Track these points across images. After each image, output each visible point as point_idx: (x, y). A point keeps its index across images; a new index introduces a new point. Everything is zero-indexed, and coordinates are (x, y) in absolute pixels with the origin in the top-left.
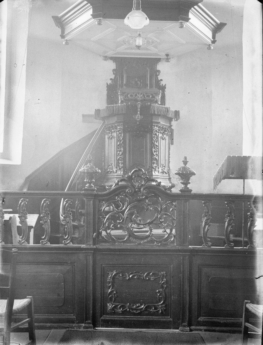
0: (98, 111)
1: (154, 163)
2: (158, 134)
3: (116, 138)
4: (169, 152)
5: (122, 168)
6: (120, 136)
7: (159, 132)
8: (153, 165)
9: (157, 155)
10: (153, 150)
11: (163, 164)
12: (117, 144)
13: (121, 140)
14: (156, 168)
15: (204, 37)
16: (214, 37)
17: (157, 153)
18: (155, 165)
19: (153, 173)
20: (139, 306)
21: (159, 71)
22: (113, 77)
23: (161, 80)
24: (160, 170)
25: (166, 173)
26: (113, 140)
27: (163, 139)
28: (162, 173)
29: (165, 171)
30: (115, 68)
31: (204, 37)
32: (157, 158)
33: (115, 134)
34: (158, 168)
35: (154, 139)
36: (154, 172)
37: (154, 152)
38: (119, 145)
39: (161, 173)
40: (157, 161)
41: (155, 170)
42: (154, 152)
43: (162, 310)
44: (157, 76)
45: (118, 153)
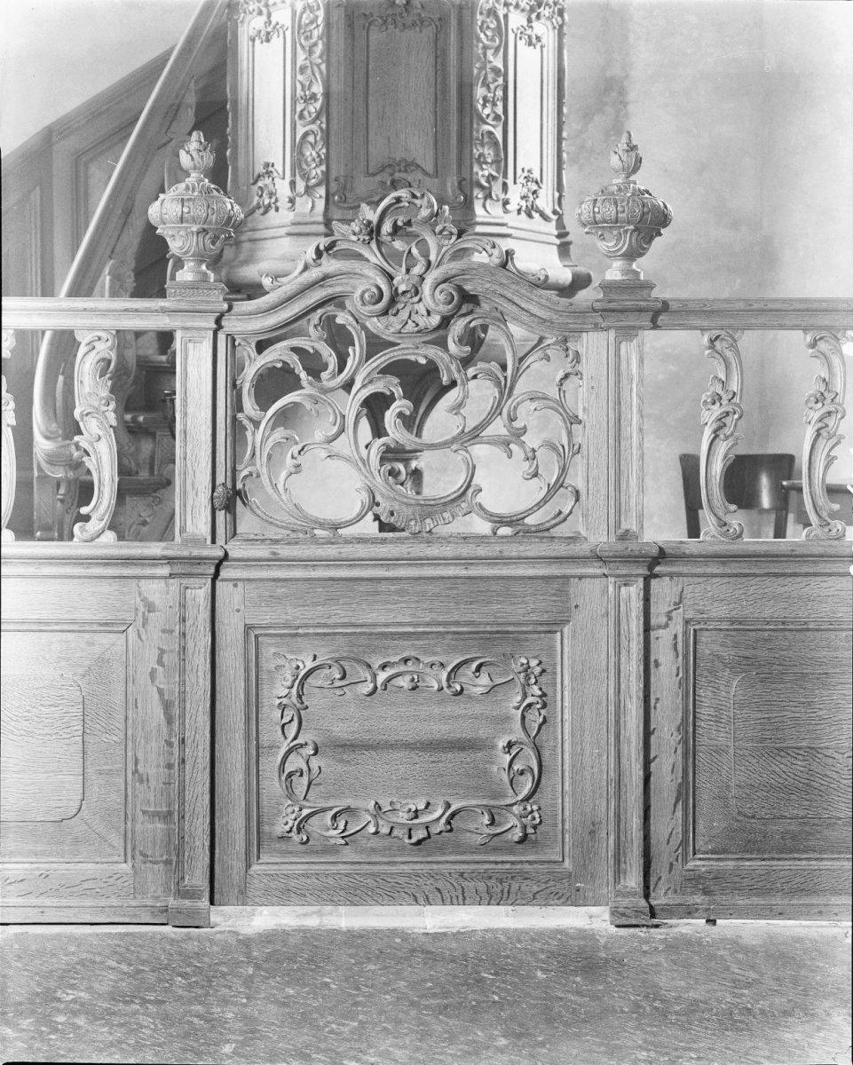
1: (481, 161)
2: (506, 16)
3: (289, 34)
5: (318, 184)
6: (311, 22)
8: (476, 169)
9: (497, 118)
10: (480, 92)
13: (315, 44)
14: (490, 188)
17: (499, 110)
18: (489, 170)
19: (479, 210)
20: (416, 814)
25: (543, 215)
26: (277, 41)
27: (530, 44)
28: (523, 213)
32: (498, 134)
35: (482, 36)
36: (484, 206)
37: (484, 106)
38: (303, 70)
39: (519, 211)
40: (497, 155)
41: (488, 196)
42: (484, 106)
43: (524, 827)
45: (299, 108)
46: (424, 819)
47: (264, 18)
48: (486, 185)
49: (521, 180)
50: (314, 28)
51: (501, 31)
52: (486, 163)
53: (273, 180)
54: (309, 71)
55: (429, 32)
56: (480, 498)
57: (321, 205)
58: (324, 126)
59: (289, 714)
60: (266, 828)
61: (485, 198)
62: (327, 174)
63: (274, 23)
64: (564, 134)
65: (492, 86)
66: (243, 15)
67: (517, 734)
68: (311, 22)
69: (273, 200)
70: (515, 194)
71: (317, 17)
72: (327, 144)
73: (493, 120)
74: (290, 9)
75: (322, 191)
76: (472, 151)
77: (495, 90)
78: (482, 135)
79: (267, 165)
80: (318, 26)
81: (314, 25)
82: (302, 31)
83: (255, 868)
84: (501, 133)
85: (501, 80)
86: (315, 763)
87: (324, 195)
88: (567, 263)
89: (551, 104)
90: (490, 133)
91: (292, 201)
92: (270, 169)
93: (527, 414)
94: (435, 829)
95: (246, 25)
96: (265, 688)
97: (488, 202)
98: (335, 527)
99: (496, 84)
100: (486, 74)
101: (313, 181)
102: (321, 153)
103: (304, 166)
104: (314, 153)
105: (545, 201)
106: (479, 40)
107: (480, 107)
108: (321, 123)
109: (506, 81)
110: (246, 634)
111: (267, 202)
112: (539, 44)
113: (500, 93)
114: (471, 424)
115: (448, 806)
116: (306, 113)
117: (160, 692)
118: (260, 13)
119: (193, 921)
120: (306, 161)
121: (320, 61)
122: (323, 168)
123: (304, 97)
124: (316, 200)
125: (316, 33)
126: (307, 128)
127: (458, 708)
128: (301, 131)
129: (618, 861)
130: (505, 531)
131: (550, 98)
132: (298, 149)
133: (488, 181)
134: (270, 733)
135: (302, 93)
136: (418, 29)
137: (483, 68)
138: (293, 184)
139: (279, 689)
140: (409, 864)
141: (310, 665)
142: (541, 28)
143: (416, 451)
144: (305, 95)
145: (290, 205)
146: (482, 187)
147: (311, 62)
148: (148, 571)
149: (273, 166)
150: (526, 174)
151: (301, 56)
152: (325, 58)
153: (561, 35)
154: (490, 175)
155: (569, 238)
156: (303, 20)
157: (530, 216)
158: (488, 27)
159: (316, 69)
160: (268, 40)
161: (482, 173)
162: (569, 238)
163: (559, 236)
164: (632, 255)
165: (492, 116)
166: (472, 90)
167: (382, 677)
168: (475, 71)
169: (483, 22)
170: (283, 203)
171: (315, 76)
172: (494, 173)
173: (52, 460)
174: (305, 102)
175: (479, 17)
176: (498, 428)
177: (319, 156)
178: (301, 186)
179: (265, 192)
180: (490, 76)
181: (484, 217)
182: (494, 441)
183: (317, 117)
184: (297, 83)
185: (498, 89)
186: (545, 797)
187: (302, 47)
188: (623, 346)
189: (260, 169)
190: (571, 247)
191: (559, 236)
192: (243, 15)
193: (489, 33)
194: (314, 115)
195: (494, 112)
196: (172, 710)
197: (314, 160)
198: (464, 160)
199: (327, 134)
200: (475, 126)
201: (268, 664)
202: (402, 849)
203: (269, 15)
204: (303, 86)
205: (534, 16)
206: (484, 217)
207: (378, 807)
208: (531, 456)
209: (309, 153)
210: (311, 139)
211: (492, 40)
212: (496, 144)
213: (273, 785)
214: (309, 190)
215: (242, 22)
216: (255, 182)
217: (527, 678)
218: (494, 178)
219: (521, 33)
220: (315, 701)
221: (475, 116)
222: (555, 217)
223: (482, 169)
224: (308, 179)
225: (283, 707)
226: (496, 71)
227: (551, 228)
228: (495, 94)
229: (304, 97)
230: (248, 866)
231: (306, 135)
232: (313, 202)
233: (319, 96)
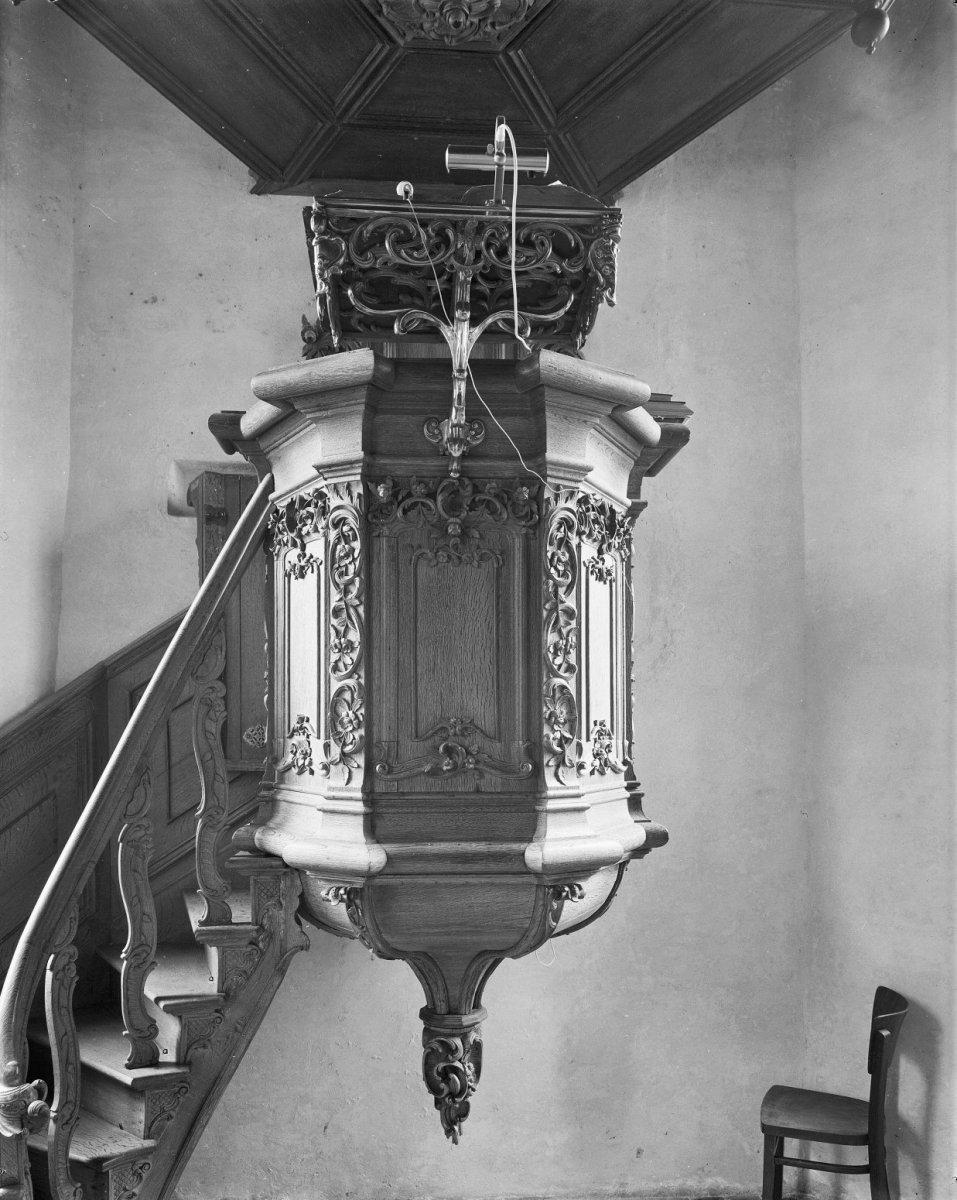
2: (579, 546)
3: (322, 567)
6: (347, 555)
7: (580, 534)
8: (546, 730)
10: (551, 638)
11: (602, 724)
13: (352, 582)
14: (563, 753)
16: (634, 490)
17: (572, 658)
24: (587, 757)
25: (615, 770)
26: (311, 578)
33: (316, 548)
34: (580, 750)
35: (553, 571)
37: (556, 654)
38: (337, 612)
39: (592, 773)
40: (570, 712)
41: (561, 762)
45: (334, 657)
47: (298, 551)
48: (559, 749)
49: (593, 736)
50: (350, 563)
51: (573, 564)
52: (557, 722)
53: (308, 737)
54: (344, 615)
58: (362, 681)
61: (558, 767)
63: (308, 556)
64: (633, 676)
65: (564, 631)
66: (278, 547)
68: (347, 555)
69: (307, 763)
70: (587, 757)
71: (354, 550)
72: (368, 703)
73: (565, 672)
74: (323, 539)
75: (360, 760)
76: (541, 709)
77: (568, 636)
78: (554, 690)
79: (301, 720)
80: (354, 560)
81: (350, 559)
82: (337, 565)
84: (574, 685)
85: (574, 623)
87: (363, 765)
88: (638, 818)
90: (563, 687)
91: (326, 767)
92: (305, 724)
95: (281, 557)
97: (561, 769)
99: (569, 628)
100: (557, 617)
101: (351, 747)
102: (359, 713)
103: (340, 729)
104: (350, 713)
105: (615, 758)
106: (550, 576)
107: (551, 657)
108: (359, 677)
109: (579, 624)
111: (301, 762)
112: (609, 578)
113: (573, 638)
116: (341, 665)
118: (295, 545)
120: (341, 723)
121: (357, 602)
122: (362, 732)
123: (339, 646)
124: (353, 769)
125: (351, 569)
126: (340, 684)
128: (335, 686)
131: (620, 638)
132: (333, 707)
133: (560, 745)
135: (337, 641)
136: (475, 563)
137: (555, 608)
138: (327, 747)
142: (610, 561)
143: (361, 127)
144: (340, 643)
145: (324, 772)
146: (554, 754)
147: (346, 604)
149: (308, 721)
150: (598, 728)
151: (335, 596)
152: (363, 599)
153: (629, 568)
154: (563, 736)
155: (639, 790)
156: (337, 552)
157: (602, 773)
158: (559, 560)
159: (352, 611)
160: (302, 576)
161: (552, 735)
162: (639, 790)
163: (628, 788)
165: (564, 666)
166: (540, 636)
168: (545, 613)
169: (553, 555)
170: (316, 767)
171: (352, 620)
172: (568, 735)
174: (339, 651)
175: (550, 550)
177: (357, 717)
178: (336, 750)
179: (299, 751)
180: (562, 619)
181: (558, 789)
183: (355, 671)
184: (332, 629)
185: (571, 635)
187: (337, 585)
189: (294, 724)
190: (642, 799)
191: (628, 788)
192: (278, 547)
193: (561, 568)
194: (350, 668)
195: (568, 662)
197: (351, 722)
198: (533, 722)
199: (368, 693)
200: (545, 679)
203: (303, 547)
204: (337, 632)
205: (605, 546)
206: (558, 789)
209: (344, 712)
210: (347, 696)
211: (564, 575)
214: (345, 757)
215: (278, 555)
216: (291, 736)
218: (568, 741)
219: (593, 566)
221: (544, 667)
222: (625, 768)
223: (554, 731)
224: (345, 745)
226: (570, 613)
227: (620, 781)
228: (567, 641)
229: (339, 646)
231: (341, 691)
232: (350, 772)
233: (356, 645)
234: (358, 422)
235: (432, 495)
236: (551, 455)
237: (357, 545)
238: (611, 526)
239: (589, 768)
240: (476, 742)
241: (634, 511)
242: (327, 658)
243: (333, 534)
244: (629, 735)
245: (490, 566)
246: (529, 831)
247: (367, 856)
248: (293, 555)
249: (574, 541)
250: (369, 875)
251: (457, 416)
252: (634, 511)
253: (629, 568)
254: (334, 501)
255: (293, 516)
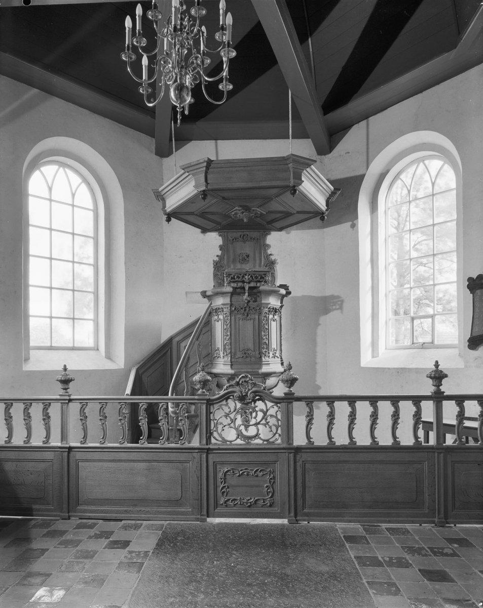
0: (214, 286)
1: (263, 348)
2: (268, 317)
4: (281, 334)
10: (263, 333)
12: (224, 327)
15: (316, 170)
16: (282, 302)
19: (263, 359)
20: (249, 500)
21: (269, 246)
22: (219, 253)
23: (271, 255)
24: (271, 355)
26: (220, 322)
29: (277, 355)
30: (221, 243)
31: (316, 170)
32: (267, 342)
33: (221, 317)
34: (269, 353)
38: (225, 329)
44: (265, 250)
46: (250, 501)
55: (252, 321)
56: (260, 436)
57: (229, 359)
59: (223, 480)
60: (218, 503)
62: (231, 352)
67: (268, 484)
70: (271, 355)
72: (231, 345)
83: (216, 510)
86: (228, 490)
89: (279, 333)
91: (223, 357)
93: (269, 419)
94: (252, 503)
96: (217, 474)
98: (231, 442)
105: (278, 354)
110: (214, 464)
114: (258, 422)
115: (254, 498)
117: (196, 475)
119: (205, 520)
127: (256, 478)
129: (289, 511)
130: (265, 442)
132: (225, 346)
134: (219, 483)
138: (224, 353)
139: (220, 475)
140: (248, 510)
141: (226, 470)
148: (194, 451)
161: (264, 351)
164: (290, 387)
167: (241, 472)
170: (222, 357)
173: (172, 412)
176: (264, 422)
178: (225, 354)
182: (262, 424)
186: (274, 498)
188: (289, 405)
196: (200, 478)
201: (218, 470)
202: (245, 507)
207: (240, 498)
208: (270, 427)
212: (267, 344)
213: (219, 494)
217: (270, 473)
220: (228, 477)
225: (221, 479)
226: (266, 329)
227: (280, 359)
230: (215, 510)
234: (229, 297)
235: (242, 309)
236: (263, 302)
237: (229, 318)
238: (275, 311)
239: (271, 357)
240: (249, 352)
241: (281, 307)
242: (224, 337)
243: (225, 316)
244: (281, 350)
245: (252, 321)
246: (261, 368)
247: (230, 371)
248: (216, 317)
249: (267, 316)
250: (232, 375)
251: (247, 294)
252: (281, 307)
253: (281, 318)
254: (225, 310)
255: (217, 311)
